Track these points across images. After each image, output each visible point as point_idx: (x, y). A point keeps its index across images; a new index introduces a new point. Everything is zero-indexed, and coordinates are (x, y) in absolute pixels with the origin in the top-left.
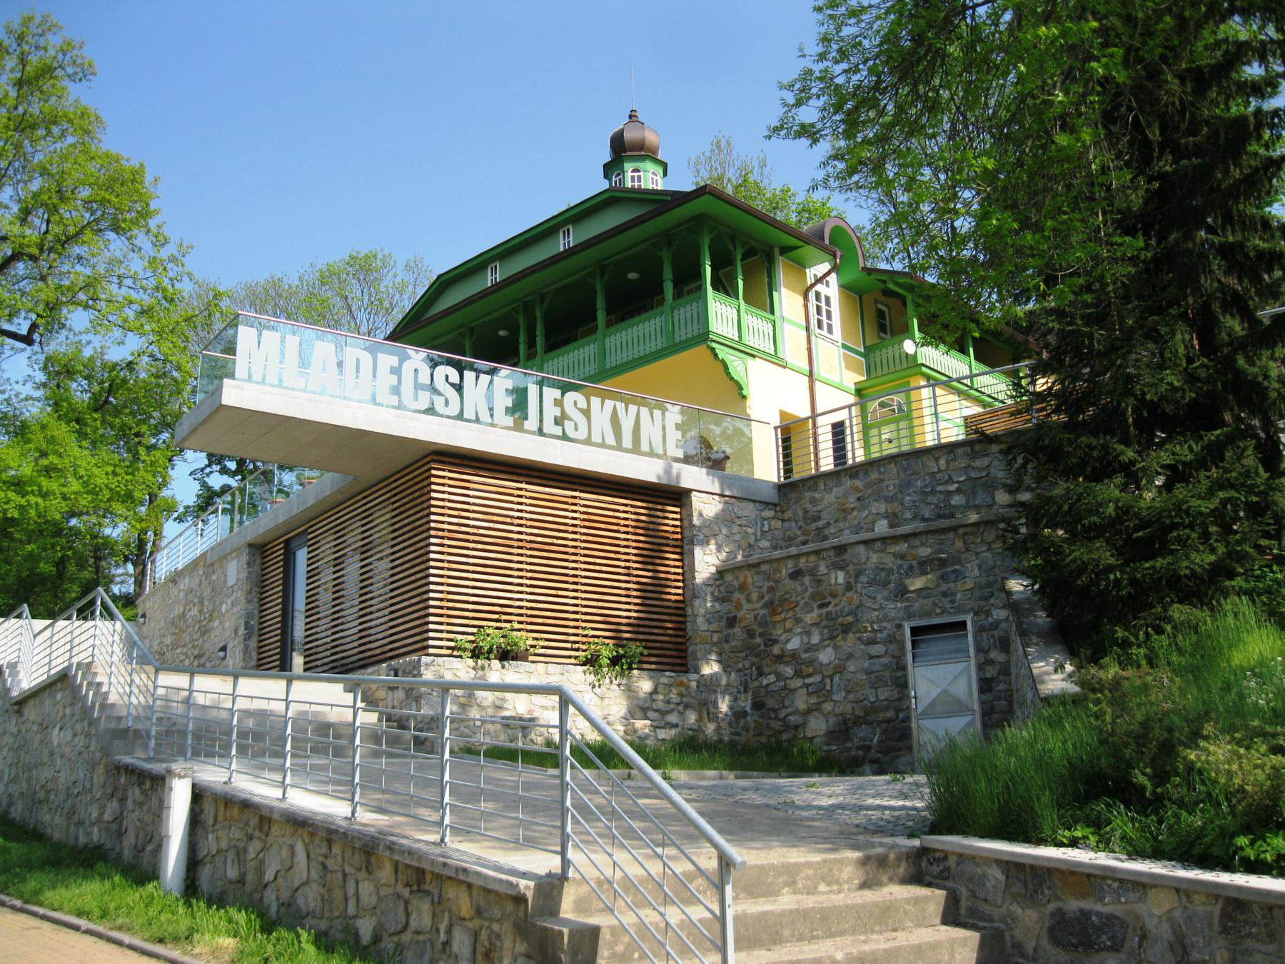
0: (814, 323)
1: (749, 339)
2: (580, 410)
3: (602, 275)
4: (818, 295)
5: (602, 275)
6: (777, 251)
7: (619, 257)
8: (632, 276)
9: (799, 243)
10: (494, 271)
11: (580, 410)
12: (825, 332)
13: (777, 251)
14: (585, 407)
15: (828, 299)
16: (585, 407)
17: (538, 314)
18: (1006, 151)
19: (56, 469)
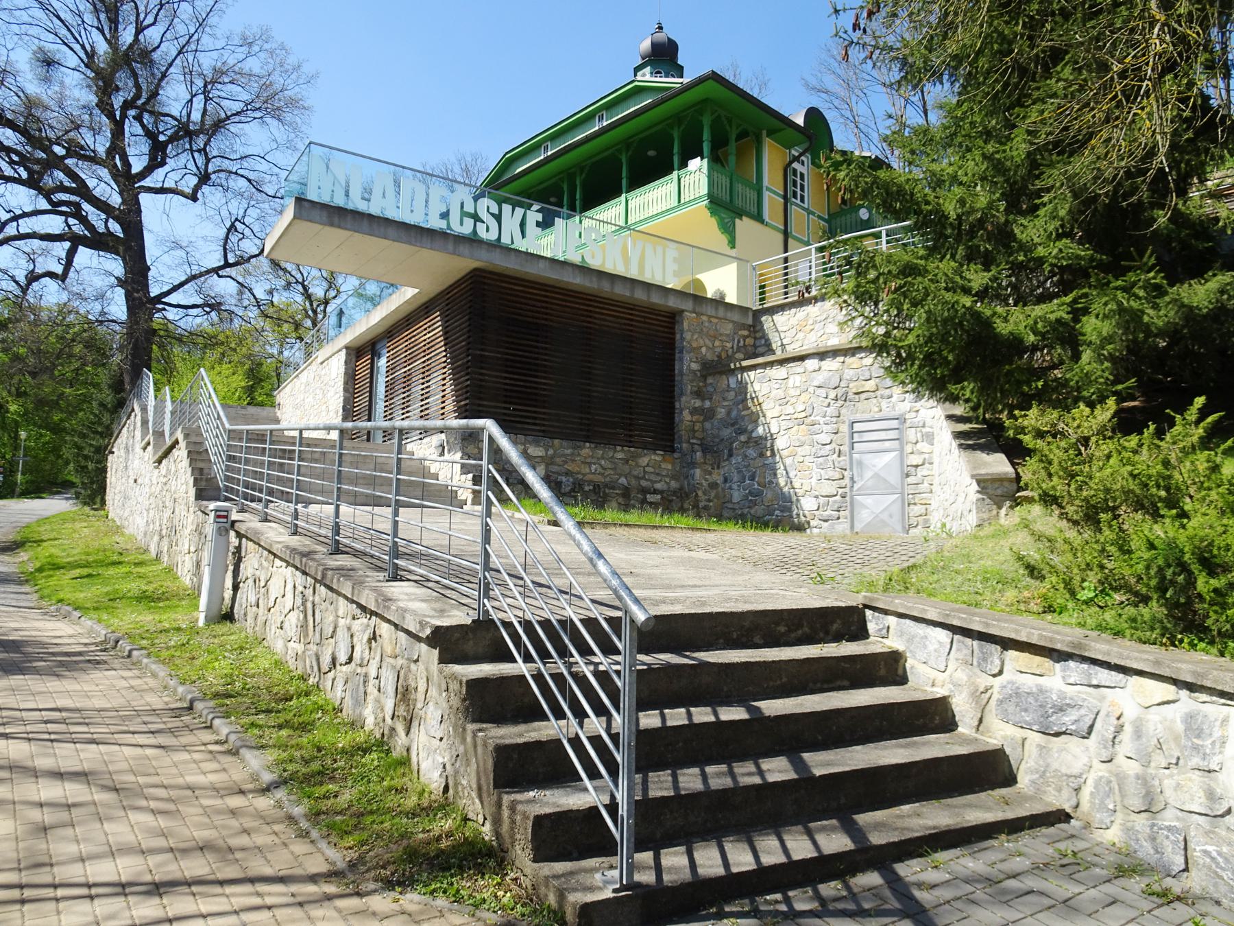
0: (790, 194)
1: (738, 202)
2: (492, 214)
3: (627, 151)
4: (795, 171)
5: (627, 151)
6: (764, 132)
7: (641, 136)
8: (651, 153)
9: (783, 126)
10: (546, 149)
11: (492, 214)
12: (798, 201)
13: (764, 132)
14: (497, 212)
15: (802, 175)
16: (497, 212)
17: (578, 182)
18: (1145, 600)
19: (1062, 433)
